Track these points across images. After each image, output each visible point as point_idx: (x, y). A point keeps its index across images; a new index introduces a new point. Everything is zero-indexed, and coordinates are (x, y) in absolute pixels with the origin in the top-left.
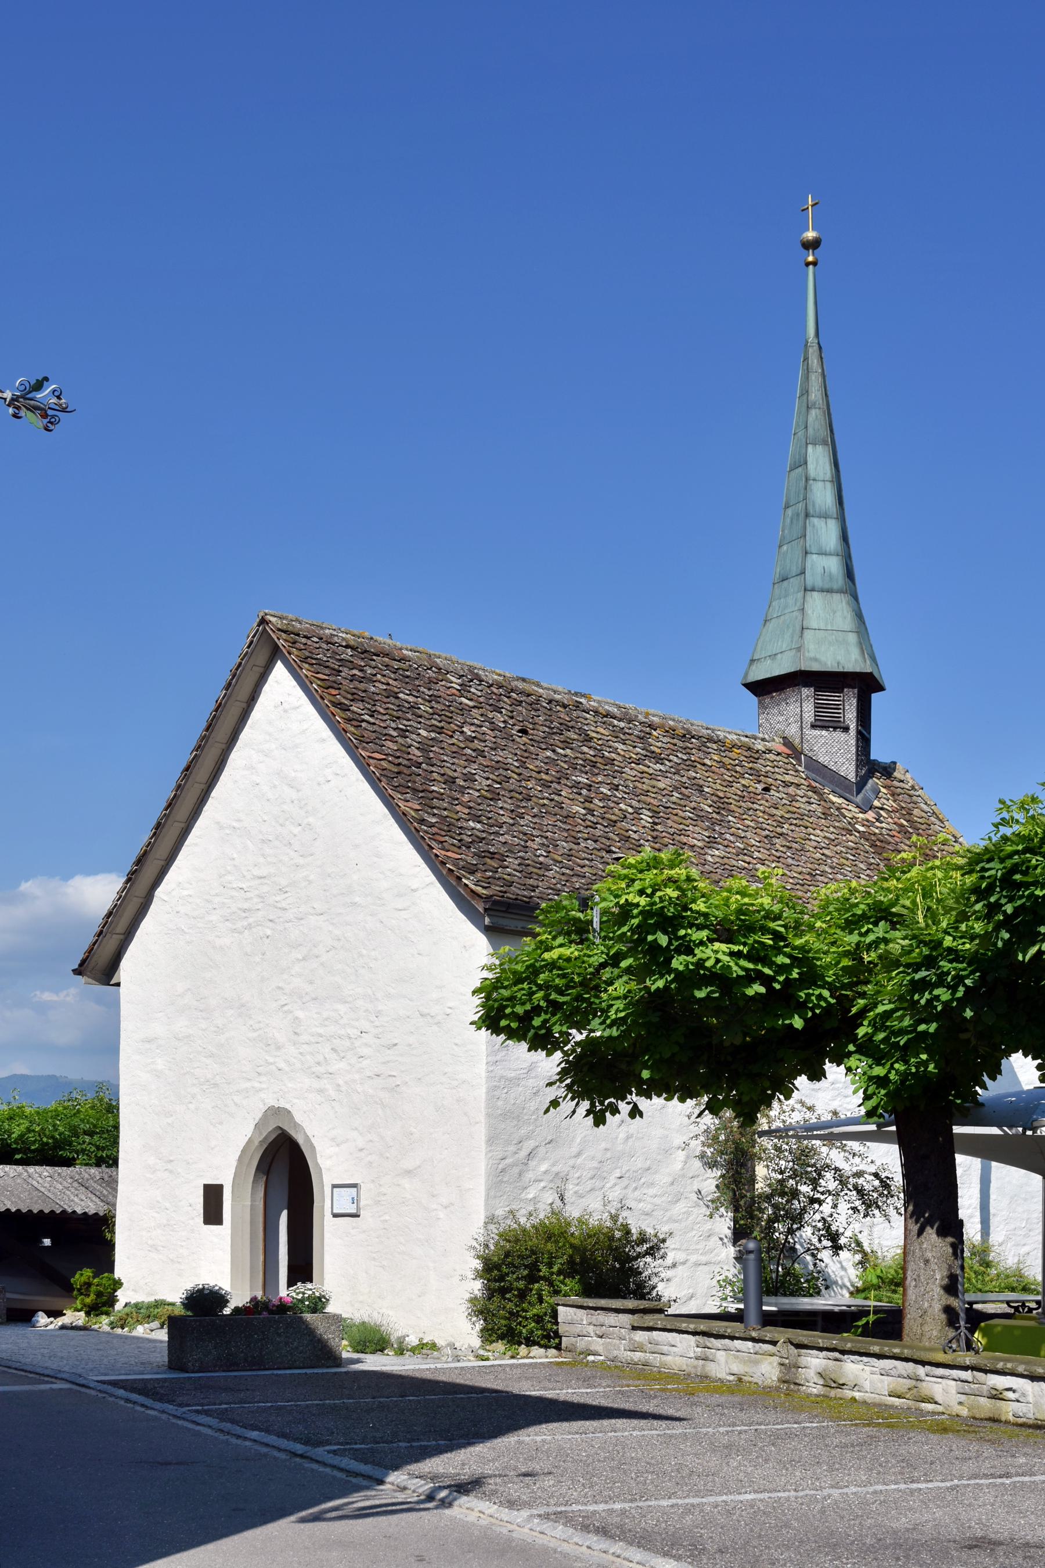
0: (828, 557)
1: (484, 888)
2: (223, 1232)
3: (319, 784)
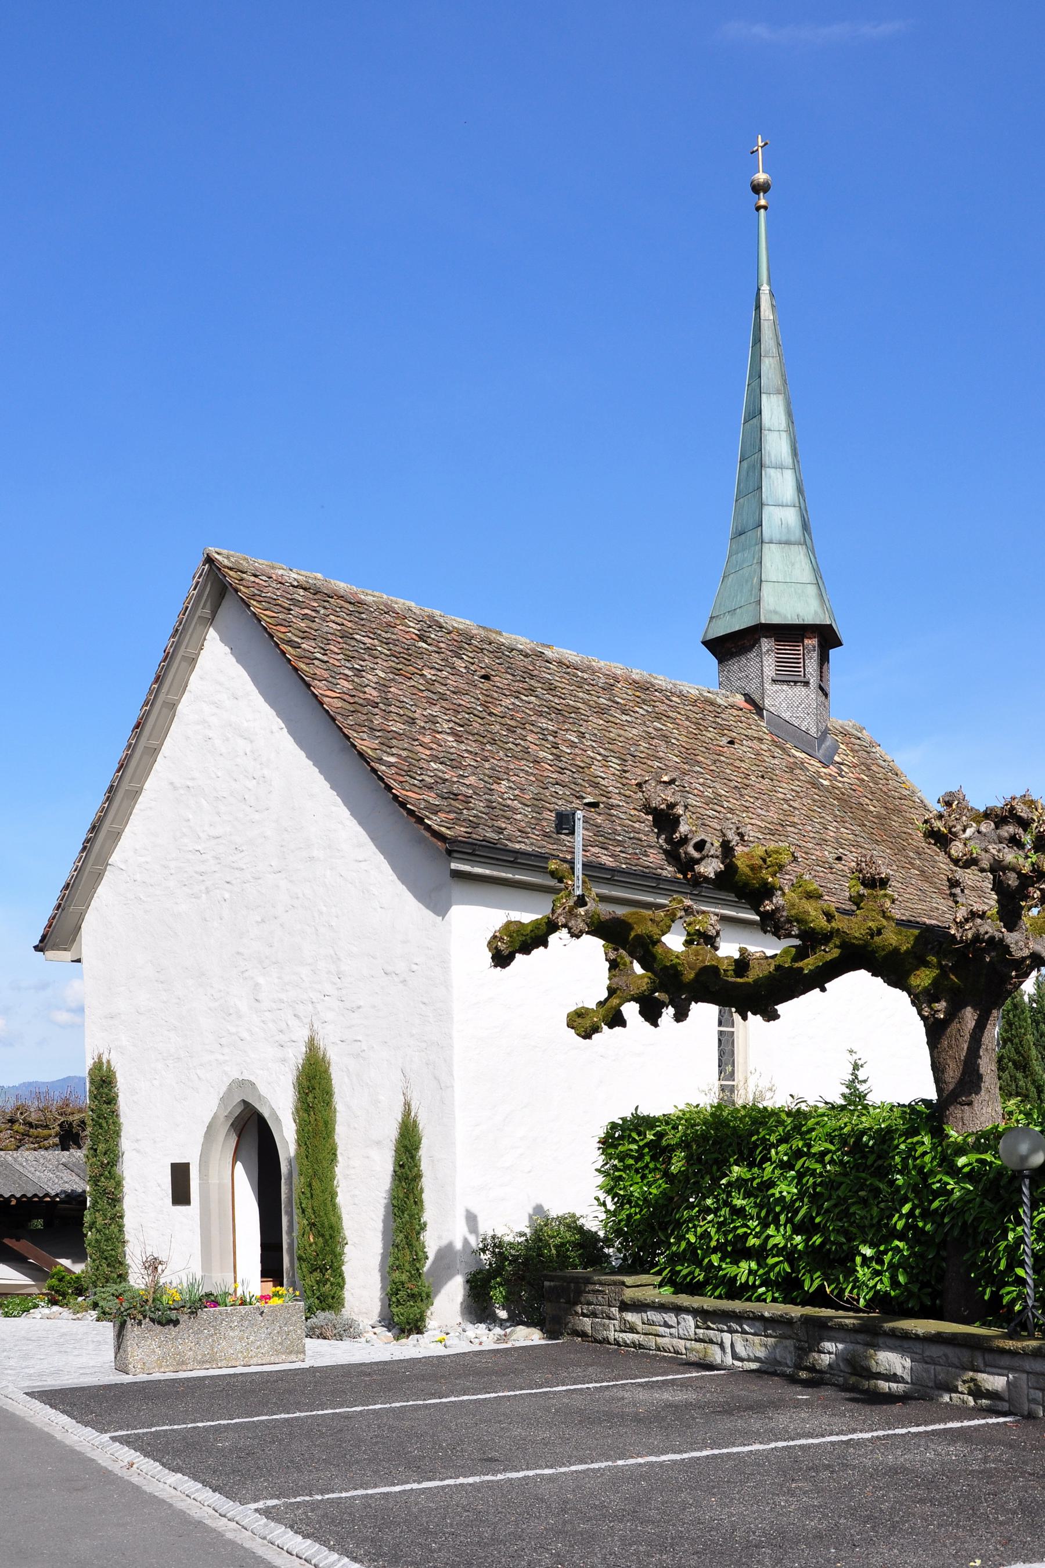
0: (785, 508)
1: (448, 828)
2: (193, 1210)
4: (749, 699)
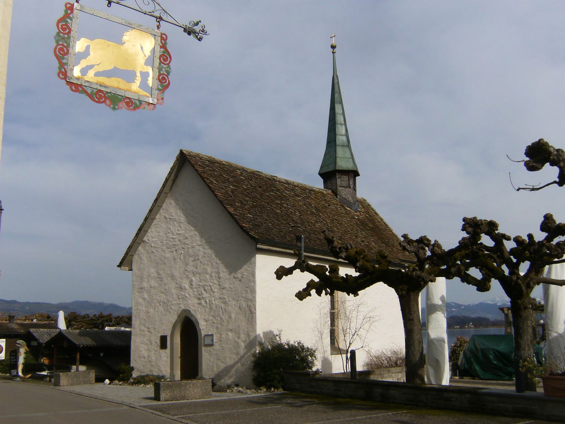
2: (168, 350)
4: (333, 192)
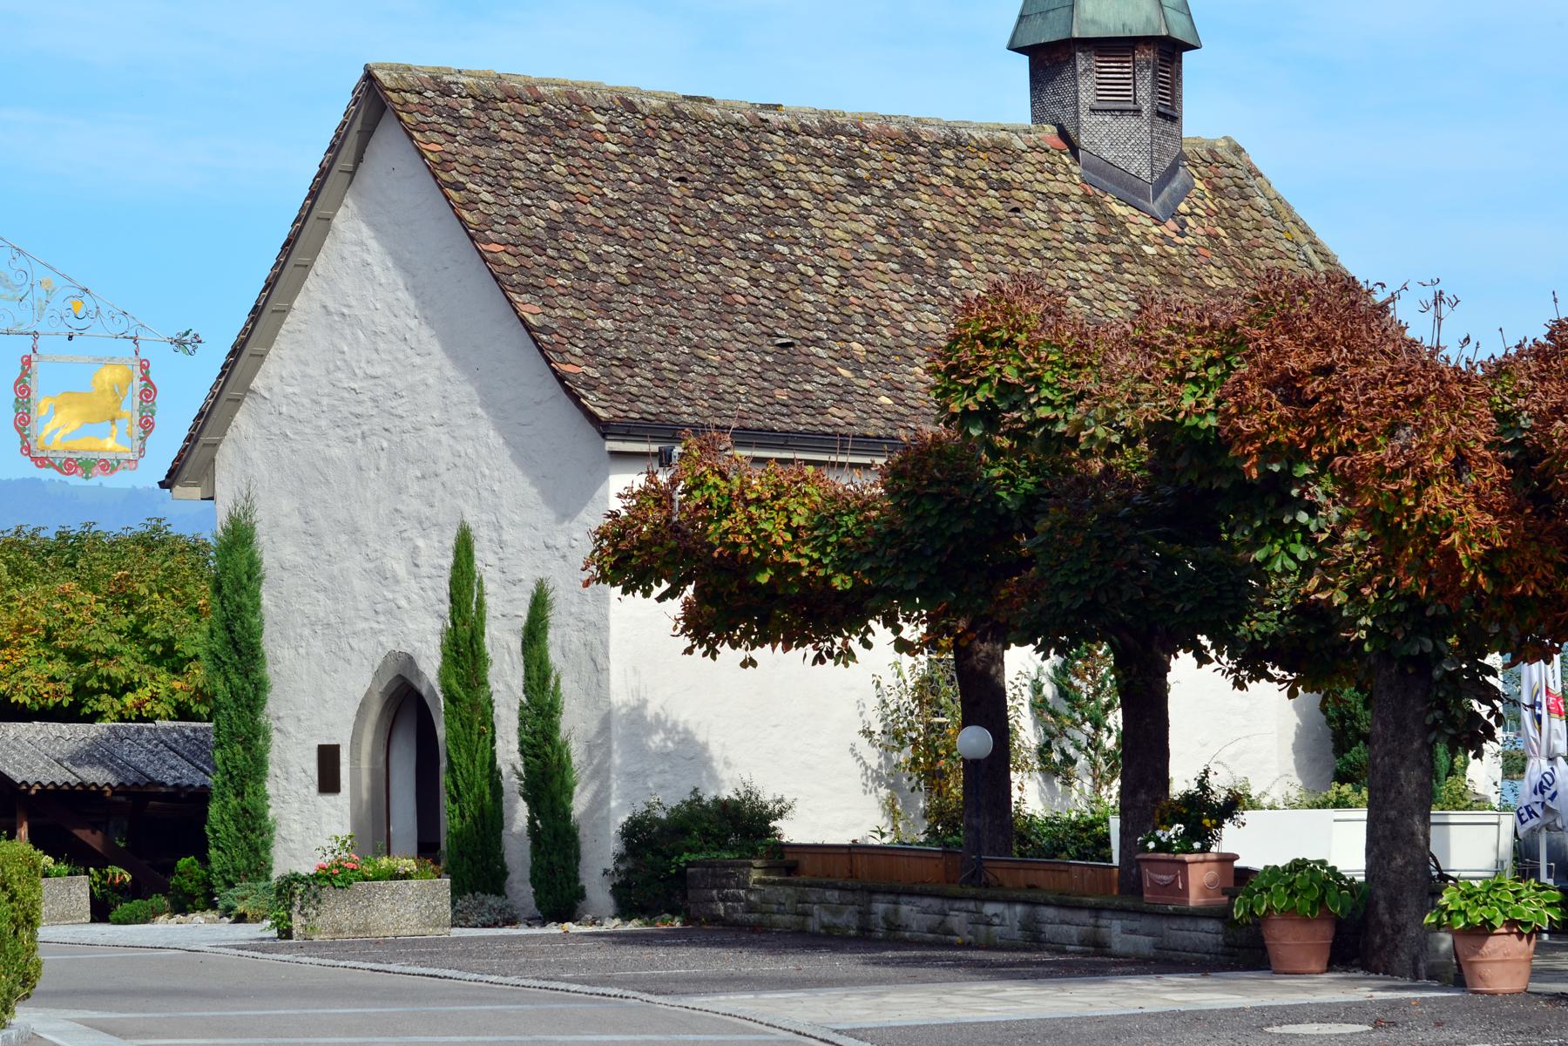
2: (343, 799)
3: (436, 270)
4: (1063, 134)
